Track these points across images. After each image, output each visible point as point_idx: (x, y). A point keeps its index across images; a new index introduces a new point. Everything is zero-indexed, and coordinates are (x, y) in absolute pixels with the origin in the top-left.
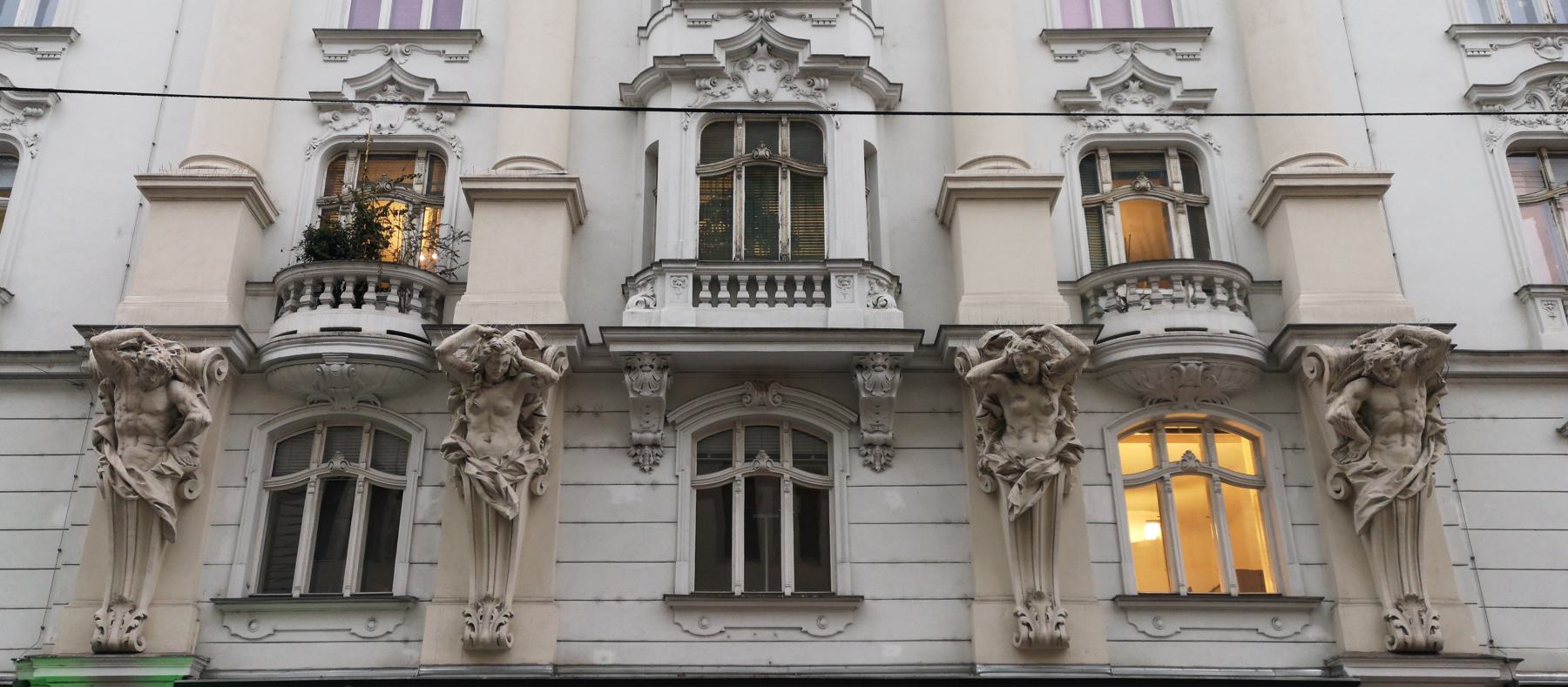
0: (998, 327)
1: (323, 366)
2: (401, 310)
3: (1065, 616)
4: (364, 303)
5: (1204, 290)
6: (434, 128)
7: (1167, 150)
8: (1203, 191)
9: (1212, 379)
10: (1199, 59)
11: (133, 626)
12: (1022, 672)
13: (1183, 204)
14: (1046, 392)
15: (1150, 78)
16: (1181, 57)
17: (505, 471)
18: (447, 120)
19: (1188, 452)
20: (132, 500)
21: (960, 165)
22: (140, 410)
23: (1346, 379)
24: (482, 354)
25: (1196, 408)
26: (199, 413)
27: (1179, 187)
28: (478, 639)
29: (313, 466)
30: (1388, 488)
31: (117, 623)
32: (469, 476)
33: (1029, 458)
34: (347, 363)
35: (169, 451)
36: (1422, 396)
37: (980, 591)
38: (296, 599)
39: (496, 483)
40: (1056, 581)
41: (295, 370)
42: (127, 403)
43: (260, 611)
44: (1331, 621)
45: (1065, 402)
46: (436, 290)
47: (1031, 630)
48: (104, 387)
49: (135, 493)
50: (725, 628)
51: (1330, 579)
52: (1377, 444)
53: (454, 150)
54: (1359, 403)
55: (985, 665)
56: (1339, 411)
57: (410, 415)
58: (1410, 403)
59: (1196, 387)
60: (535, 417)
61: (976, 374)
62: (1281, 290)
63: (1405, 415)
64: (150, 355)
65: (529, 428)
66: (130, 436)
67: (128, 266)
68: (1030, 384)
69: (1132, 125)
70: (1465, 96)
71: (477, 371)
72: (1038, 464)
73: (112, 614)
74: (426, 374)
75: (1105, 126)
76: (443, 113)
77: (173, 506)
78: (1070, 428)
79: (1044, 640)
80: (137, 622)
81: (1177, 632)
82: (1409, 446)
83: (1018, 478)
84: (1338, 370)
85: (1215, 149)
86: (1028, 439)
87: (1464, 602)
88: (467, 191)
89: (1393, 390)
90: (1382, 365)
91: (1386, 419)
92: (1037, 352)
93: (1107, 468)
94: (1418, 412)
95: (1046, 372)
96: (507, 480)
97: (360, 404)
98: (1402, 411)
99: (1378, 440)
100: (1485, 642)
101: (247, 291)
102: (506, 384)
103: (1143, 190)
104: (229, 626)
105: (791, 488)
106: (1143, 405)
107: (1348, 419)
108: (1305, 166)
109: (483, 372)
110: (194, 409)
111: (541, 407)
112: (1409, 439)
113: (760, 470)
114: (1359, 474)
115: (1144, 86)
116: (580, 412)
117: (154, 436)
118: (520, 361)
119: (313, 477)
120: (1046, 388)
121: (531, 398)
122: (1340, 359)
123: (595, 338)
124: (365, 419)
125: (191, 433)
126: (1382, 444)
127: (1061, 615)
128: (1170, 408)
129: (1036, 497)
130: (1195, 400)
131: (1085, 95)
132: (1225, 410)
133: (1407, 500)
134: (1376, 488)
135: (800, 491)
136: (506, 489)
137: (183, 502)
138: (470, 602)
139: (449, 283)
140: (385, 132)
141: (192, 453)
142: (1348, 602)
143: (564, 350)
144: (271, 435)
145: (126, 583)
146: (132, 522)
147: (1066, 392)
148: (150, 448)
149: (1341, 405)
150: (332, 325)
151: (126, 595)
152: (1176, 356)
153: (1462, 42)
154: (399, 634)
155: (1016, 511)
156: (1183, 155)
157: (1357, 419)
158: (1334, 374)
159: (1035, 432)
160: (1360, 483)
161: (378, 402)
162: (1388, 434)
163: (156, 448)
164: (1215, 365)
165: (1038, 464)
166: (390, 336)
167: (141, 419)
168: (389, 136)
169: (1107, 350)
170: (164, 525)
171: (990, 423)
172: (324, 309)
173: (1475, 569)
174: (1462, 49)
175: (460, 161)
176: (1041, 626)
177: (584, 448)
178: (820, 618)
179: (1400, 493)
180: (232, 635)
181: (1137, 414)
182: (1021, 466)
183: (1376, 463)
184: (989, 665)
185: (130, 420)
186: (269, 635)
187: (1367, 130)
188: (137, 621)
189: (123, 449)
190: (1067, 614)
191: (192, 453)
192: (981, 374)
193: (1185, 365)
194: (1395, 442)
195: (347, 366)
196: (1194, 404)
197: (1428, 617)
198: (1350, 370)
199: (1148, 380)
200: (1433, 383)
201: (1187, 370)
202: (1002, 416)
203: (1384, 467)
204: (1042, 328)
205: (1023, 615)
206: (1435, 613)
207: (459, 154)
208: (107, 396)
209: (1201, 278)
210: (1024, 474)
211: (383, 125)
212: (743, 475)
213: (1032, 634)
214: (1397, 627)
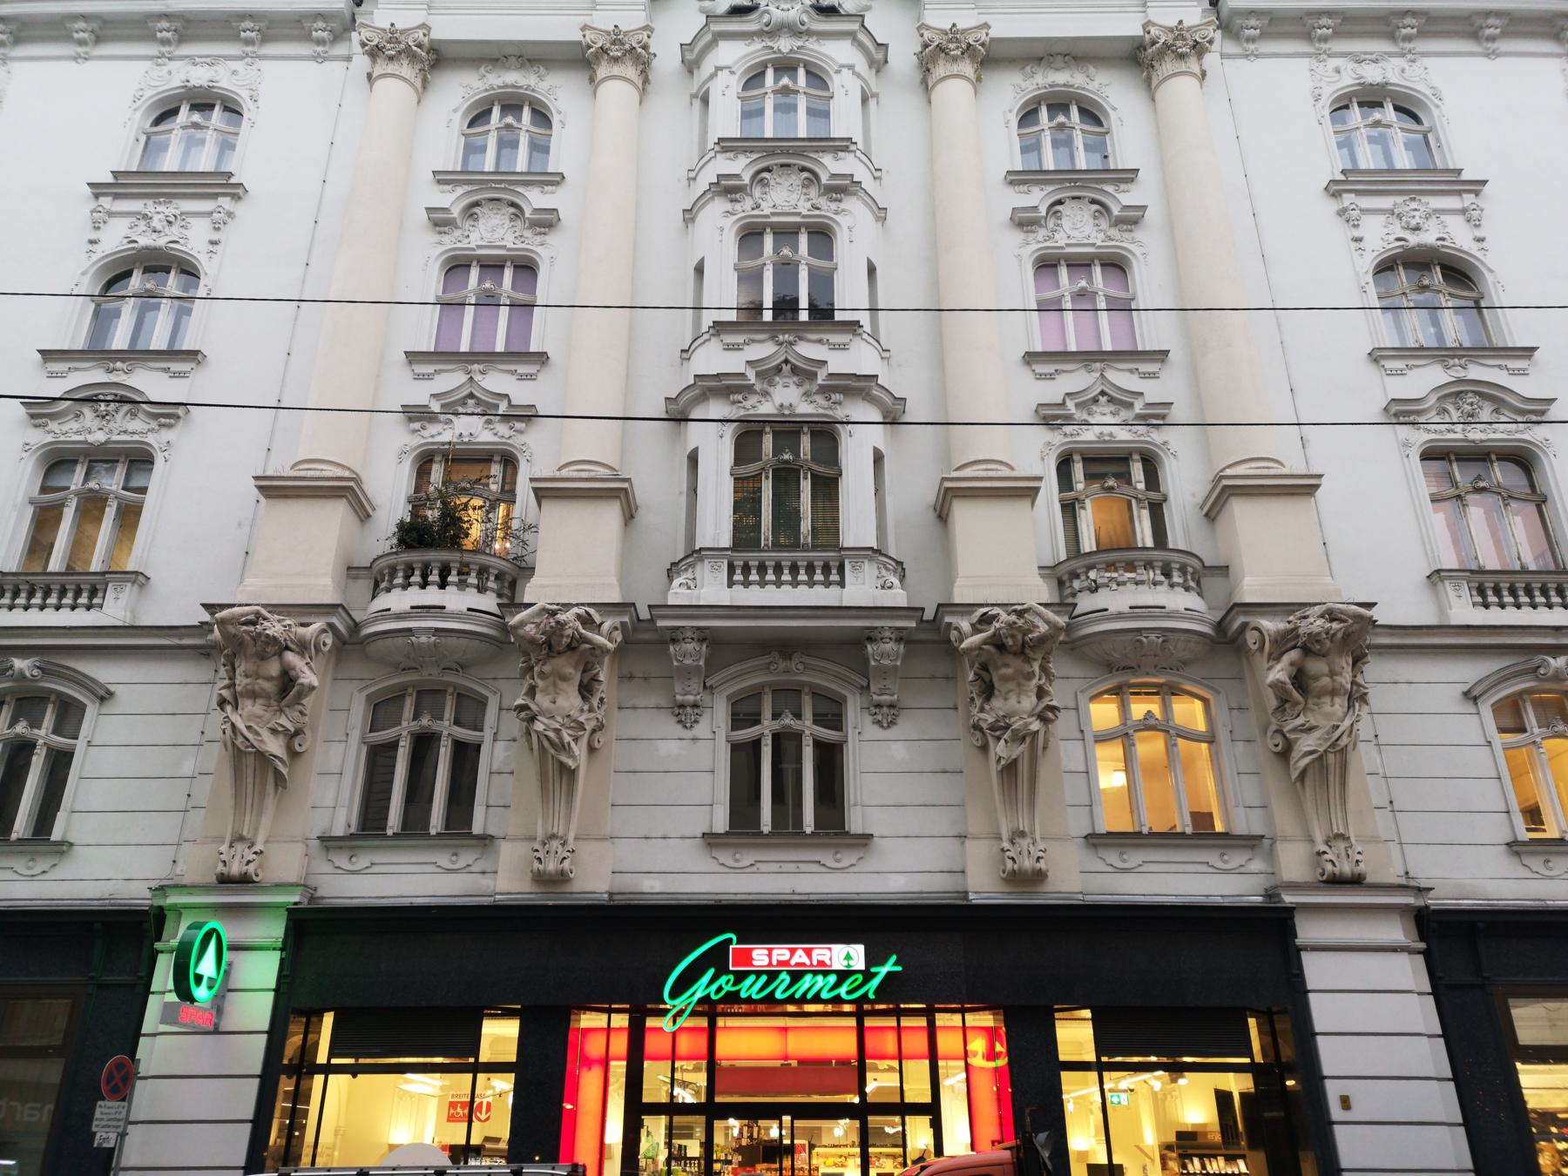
0: (987, 605)
2: (479, 591)
5: (1163, 574)
14: (1028, 660)
19: (1149, 712)
20: (251, 753)
24: (548, 628)
27: (1141, 486)
28: (544, 871)
29: (404, 724)
31: (238, 857)
35: (281, 711)
36: (1348, 664)
38: (767, 835)
39: (561, 738)
41: (389, 642)
44: (1271, 855)
48: (227, 656)
49: (253, 746)
51: (1270, 820)
54: (1294, 670)
56: (1277, 676)
58: (1337, 669)
63: (1334, 681)
66: (249, 697)
68: (1015, 654)
69: (1101, 433)
71: (544, 643)
72: (1021, 722)
77: (285, 757)
79: (1026, 872)
81: (1140, 865)
82: (1337, 706)
86: (1013, 701)
94: (1345, 678)
98: (1331, 677)
99: (1310, 701)
100: (1402, 873)
103: (1111, 489)
105: (811, 742)
106: (1111, 672)
111: (598, 673)
112: (1337, 700)
114: (1294, 730)
115: (1112, 400)
116: (631, 678)
117: (268, 697)
118: (581, 635)
119: (405, 733)
121: (589, 666)
124: (449, 684)
129: (1019, 750)
132: (1181, 676)
133: (1335, 753)
134: (1309, 743)
136: (569, 744)
137: (294, 754)
139: (520, 568)
140: (466, 440)
141: (302, 713)
142: (1285, 839)
144: (369, 697)
146: (250, 772)
151: (245, 833)
152: (1139, 630)
153: (1382, 363)
154: (477, 867)
155: (1003, 762)
159: (1019, 695)
162: (1319, 696)
165: (1021, 722)
166: (470, 613)
168: (469, 443)
170: (277, 773)
176: (1024, 860)
177: (635, 708)
181: (1105, 680)
186: (367, 868)
189: (243, 709)
191: (302, 713)
193: (1147, 637)
195: (433, 638)
201: (1149, 642)
202: (991, 680)
204: (1025, 606)
209: (1160, 564)
210: (1009, 731)
211: (464, 433)
213: (541, 867)
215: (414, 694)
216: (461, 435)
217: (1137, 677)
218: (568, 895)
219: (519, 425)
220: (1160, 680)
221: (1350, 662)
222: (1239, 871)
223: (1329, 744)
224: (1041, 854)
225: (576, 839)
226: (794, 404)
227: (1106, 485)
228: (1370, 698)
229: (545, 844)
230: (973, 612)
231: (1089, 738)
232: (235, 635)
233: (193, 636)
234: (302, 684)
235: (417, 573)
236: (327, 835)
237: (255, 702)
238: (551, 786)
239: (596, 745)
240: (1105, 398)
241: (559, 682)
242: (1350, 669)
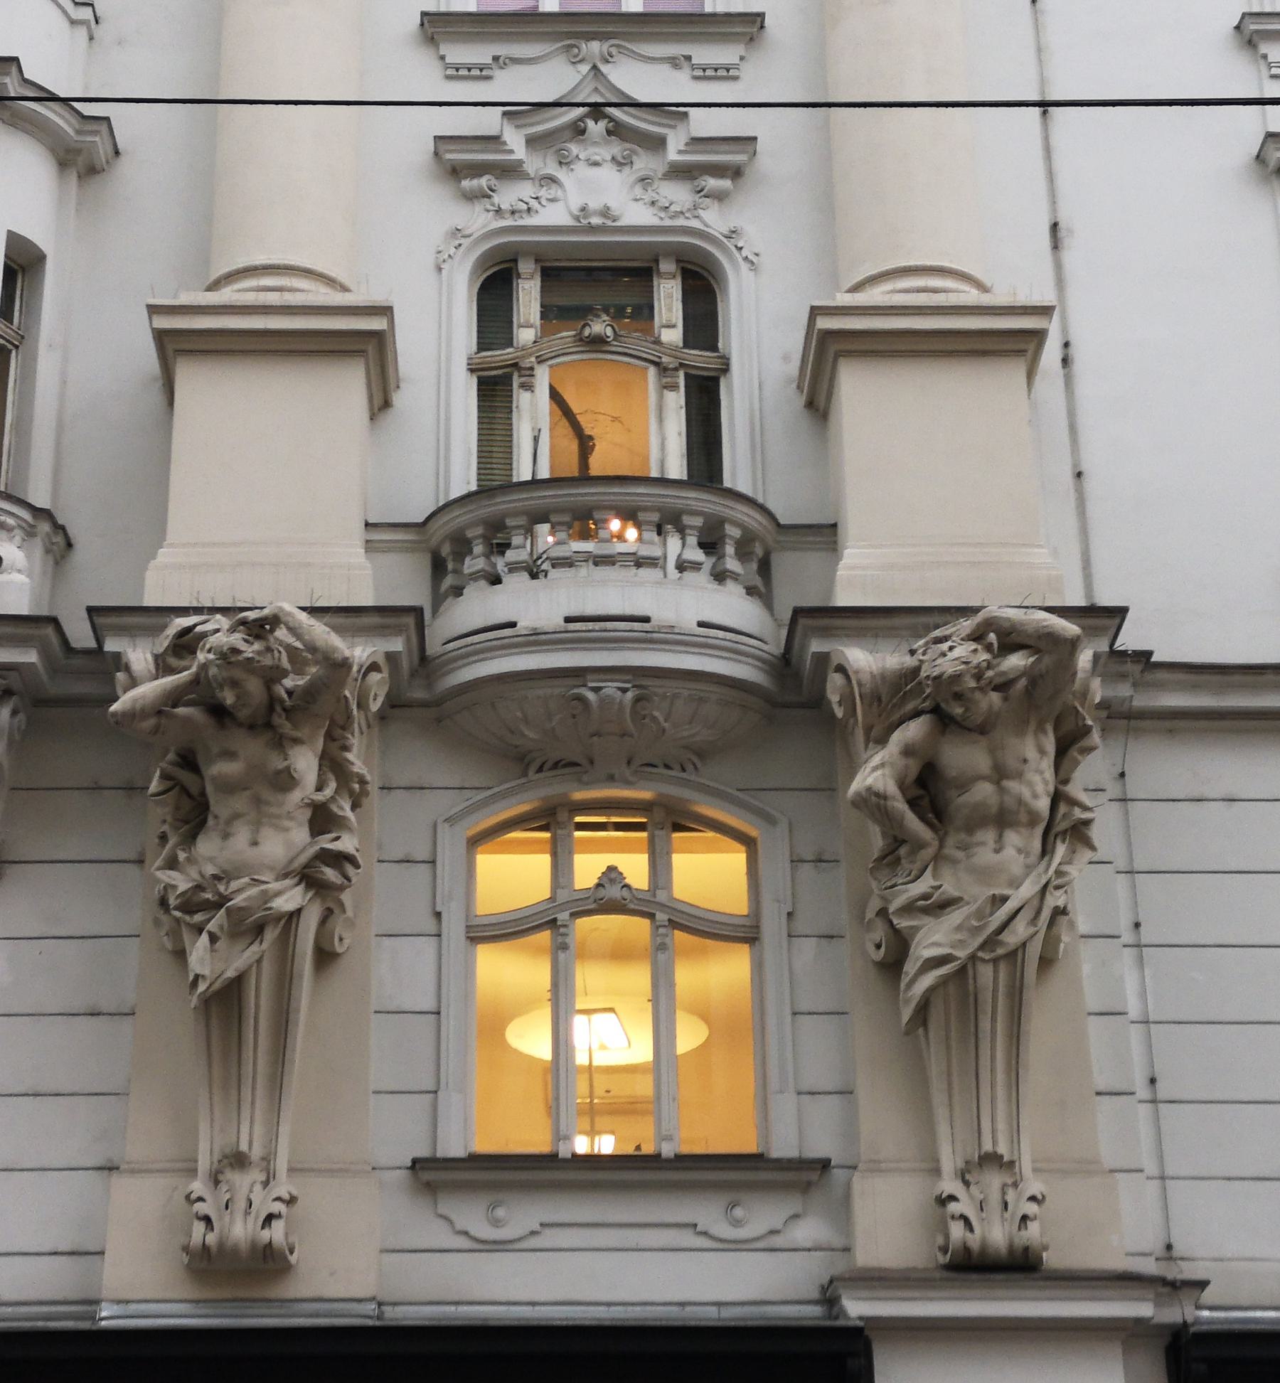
0: (198, 610)
3: (291, 1201)
5: (702, 545)
7: (657, 261)
8: (720, 345)
9: (654, 719)
10: (736, 78)
12: (236, 1316)
13: (676, 369)
14: (281, 743)
16: (700, 73)
19: (611, 869)
21: (849, 285)
23: (896, 717)
25: (631, 779)
27: (673, 336)
30: (959, 936)
33: (239, 878)
36: (1042, 752)
37: (135, 1150)
40: (285, 1129)
44: (843, 1211)
45: (332, 764)
46: (763, 541)
47: (212, 1229)
50: (542, 1225)
51: (850, 1130)
52: (949, 850)
54: (914, 767)
55: (119, 1302)
56: (869, 781)
58: (1011, 763)
59: (623, 735)
61: (128, 706)
62: (835, 542)
63: (1002, 790)
68: (252, 727)
69: (583, 209)
70: (1258, 156)
72: (254, 891)
73: (224, 1187)
75: (529, 209)
78: (344, 818)
79: (235, 1251)
81: (533, 1233)
82: (1009, 852)
83: (209, 920)
84: (880, 700)
85: (746, 258)
86: (241, 837)
87: (1107, 1166)
88: (161, 337)
89: (981, 738)
90: (949, 686)
91: (965, 798)
92: (248, 659)
93: (434, 904)
94: (1030, 785)
95: (282, 701)
98: (998, 783)
99: (951, 841)
100: (1159, 1250)
103: (597, 342)
104: (453, 1217)
106: (525, 774)
107: (885, 798)
108: (889, 292)
112: (1013, 838)
114: (909, 909)
115: (617, 131)
120: (281, 737)
122: (883, 676)
123: (80, 633)
126: (958, 848)
127: (278, 1199)
128: (580, 781)
129: (239, 959)
130: (629, 763)
131: (491, 146)
132: (686, 783)
133: (995, 961)
134: (936, 938)
142: (876, 1168)
143: (381, 661)
147: (336, 744)
149: (875, 769)
152: (578, 673)
153: (1264, 48)
155: (202, 987)
156: (691, 271)
157: (912, 803)
158: (871, 705)
159: (257, 825)
160: (912, 927)
162: (970, 828)
164: (660, 691)
165: (254, 891)
169: (456, 659)
171: (177, 808)
173: (1154, 1101)
174: (1262, 62)
176: (232, 1222)
178: (734, 1205)
179: (982, 947)
181: (503, 796)
182: (220, 895)
183: (940, 886)
184: (128, 1302)
187: (1055, 227)
192: (138, 706)
193: (596, 690)
194: (983, 844)
196: (627, 772)
197: (1020, 1196)
198: (904, 700)
199: (526, 721)
200: (1068, 726)
201: (601, 701)
202: (203, 793)
203: (956, 894)
204: (266, 612)
205: (201, 1199)
206: (1035, 1187)
209: (698, 521)
210: (223, 910)
213: (211, 1239)
214: (953, 1217)
217: (587, 785)
220: (645, 795)
221: (1050, 744)
222: (766, 1244)
223: (980, 940)
224: (278, 1207)
226: (613, 204)
227: (587, 332)
228: (1095, 833)
230: (165, 627)
231: (454, 928)
240: (602, 125)
242: (1047, 764)
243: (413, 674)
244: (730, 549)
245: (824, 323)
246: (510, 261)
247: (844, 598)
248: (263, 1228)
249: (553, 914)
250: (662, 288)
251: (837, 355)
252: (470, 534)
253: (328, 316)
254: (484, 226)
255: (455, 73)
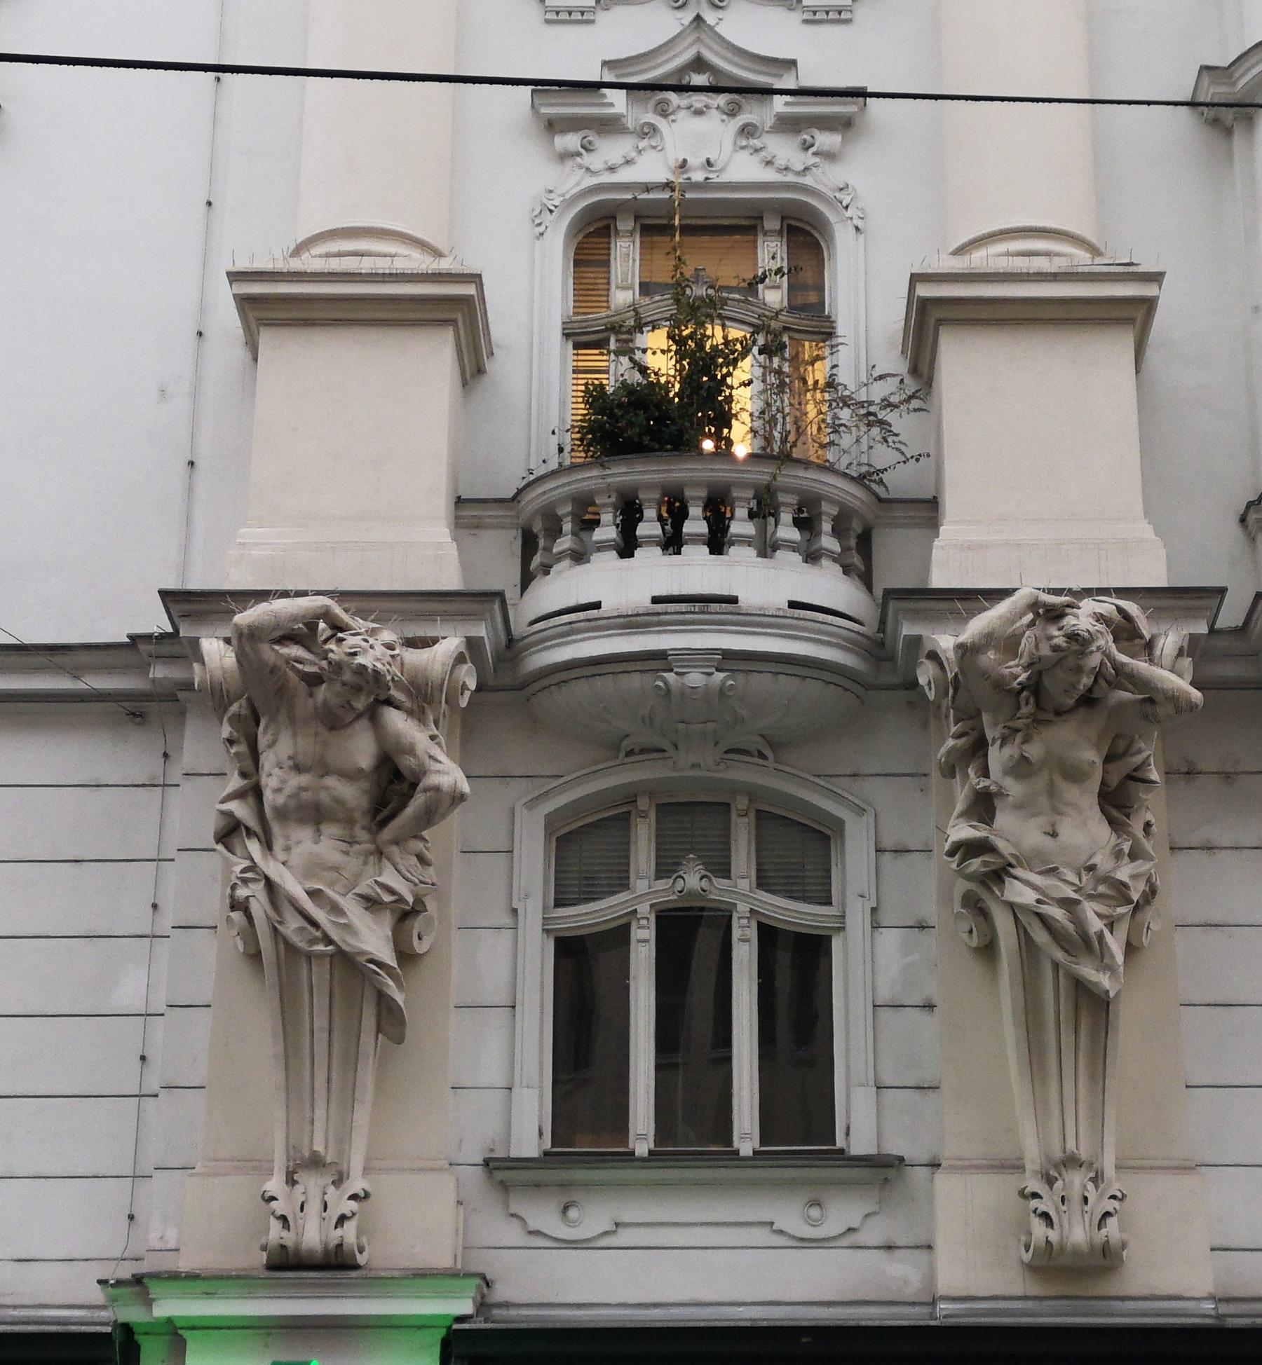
1: (670, 676)
2: (763, 553)
4: (732, 544)
6: (799, 167)
10: (847, 21)
11: (349, 1214)
15: (737, 65)
17: (1091, 897)
18: (826, 148)
20: (321, 955)
22: (324, 768)
24: (1045, 651)
26: (448, 773)
28: (1062, 1248)
29: (641, 885)
31: (314, 1208)
32: (1012, 906)
34: (718, 670)
35: (380, 853)
38: (642, 1160)
39: (1079, 923)
41: (605, 685)
42: (296, 753)
43: (587, 1185)
48: (236, 720)
49: (329, 941)
53: (849, 213)
57: (833, 779)
60: (1132, 784)
64: (355, 654)
65: (1119, 807)
66: (301, 821)
67: (192, 464)
71: (1023, 687)
73: (299, 1188)
74: (860, 691)
76: (816, 133)
77: (393, 963)
80: (353, 1205)
96: (1099, 916)
97: (730, 756)
101: (457, 517)
102: (1082, 712)
105: (753, 933)
109: (1035, 687)
110: (437, 766)
111: (1145, 763)
113: (684, 894)
116: (1191, 773)
117: (349, 822)
118: (1119, 668)
119: (644, 909)
121: (1122, 745)
124: (736, 789)
125: (429, 816)
135: (768, 935)
136: (1101, 936)
137: (406, 956)
138: (1028, 1166)
139: (880, 500)
140: (698, 176)
141: (421, 859)
144: (550, 821)
145: (317, 1124)
146: (321, 1002)
148: (344, 846)
150: (676, 591)
151: (319, 1147)
154: (873, 1234)
161: (768, 752)
163: (357, 847)
166: (659, 607)
167: (327, 788)
168: (706, 185)
170: (383, 999)
172: (649, 558)
175: (862, 237)
177: (1210, 848)
180: (530, 1233)
185: (305, 789)
186: (606, 1233)
188: (352, 1202)
189: (287, 849)
190: (1124, 1196)
191: (421, 859)
195: (720, 676)
207: (860, 223)
208: (242, 739)
211: (692, 161)
212: (652, 906)
213: (1053, 1236)
215: (652, 815)
216: (684, 165)
218: (1119, 1304)
219: (826, 140)
224: (1111, 1205)
225: (1117, 1167)
229: (1050, 1181)
232: (274, 670)
233: (110, 670)
234: (437, 789)
235: (695, 511)
236: (499, 1154)
237: (318, 832)
238: (1052, 1043)
239: (420, 947)
241: (1061, 784)
243: (499, 658)
244: (827, 526)
245: (924, 291)
246: (756, 218)
247: (938, 580)
248: (336, 1228)
249: (632, 906)
250: (618, 246)
251: (940, 322)
252: (560, 512)
253: (928, 284)
254: (578, 184)
255: (556, 17)
